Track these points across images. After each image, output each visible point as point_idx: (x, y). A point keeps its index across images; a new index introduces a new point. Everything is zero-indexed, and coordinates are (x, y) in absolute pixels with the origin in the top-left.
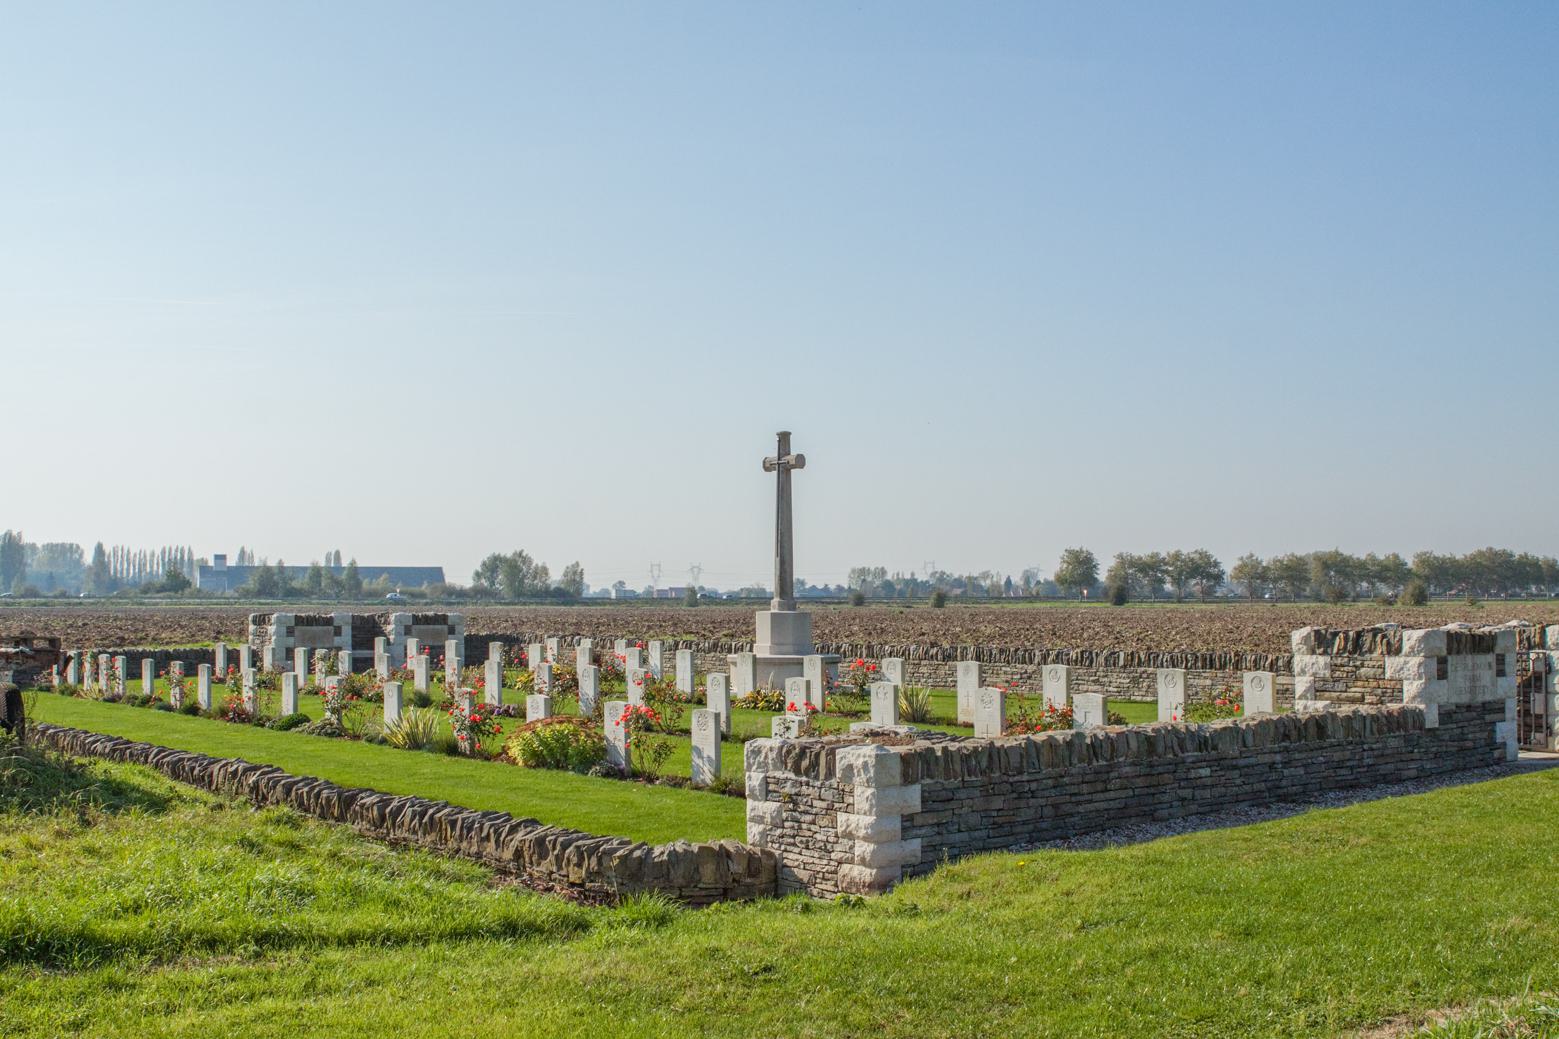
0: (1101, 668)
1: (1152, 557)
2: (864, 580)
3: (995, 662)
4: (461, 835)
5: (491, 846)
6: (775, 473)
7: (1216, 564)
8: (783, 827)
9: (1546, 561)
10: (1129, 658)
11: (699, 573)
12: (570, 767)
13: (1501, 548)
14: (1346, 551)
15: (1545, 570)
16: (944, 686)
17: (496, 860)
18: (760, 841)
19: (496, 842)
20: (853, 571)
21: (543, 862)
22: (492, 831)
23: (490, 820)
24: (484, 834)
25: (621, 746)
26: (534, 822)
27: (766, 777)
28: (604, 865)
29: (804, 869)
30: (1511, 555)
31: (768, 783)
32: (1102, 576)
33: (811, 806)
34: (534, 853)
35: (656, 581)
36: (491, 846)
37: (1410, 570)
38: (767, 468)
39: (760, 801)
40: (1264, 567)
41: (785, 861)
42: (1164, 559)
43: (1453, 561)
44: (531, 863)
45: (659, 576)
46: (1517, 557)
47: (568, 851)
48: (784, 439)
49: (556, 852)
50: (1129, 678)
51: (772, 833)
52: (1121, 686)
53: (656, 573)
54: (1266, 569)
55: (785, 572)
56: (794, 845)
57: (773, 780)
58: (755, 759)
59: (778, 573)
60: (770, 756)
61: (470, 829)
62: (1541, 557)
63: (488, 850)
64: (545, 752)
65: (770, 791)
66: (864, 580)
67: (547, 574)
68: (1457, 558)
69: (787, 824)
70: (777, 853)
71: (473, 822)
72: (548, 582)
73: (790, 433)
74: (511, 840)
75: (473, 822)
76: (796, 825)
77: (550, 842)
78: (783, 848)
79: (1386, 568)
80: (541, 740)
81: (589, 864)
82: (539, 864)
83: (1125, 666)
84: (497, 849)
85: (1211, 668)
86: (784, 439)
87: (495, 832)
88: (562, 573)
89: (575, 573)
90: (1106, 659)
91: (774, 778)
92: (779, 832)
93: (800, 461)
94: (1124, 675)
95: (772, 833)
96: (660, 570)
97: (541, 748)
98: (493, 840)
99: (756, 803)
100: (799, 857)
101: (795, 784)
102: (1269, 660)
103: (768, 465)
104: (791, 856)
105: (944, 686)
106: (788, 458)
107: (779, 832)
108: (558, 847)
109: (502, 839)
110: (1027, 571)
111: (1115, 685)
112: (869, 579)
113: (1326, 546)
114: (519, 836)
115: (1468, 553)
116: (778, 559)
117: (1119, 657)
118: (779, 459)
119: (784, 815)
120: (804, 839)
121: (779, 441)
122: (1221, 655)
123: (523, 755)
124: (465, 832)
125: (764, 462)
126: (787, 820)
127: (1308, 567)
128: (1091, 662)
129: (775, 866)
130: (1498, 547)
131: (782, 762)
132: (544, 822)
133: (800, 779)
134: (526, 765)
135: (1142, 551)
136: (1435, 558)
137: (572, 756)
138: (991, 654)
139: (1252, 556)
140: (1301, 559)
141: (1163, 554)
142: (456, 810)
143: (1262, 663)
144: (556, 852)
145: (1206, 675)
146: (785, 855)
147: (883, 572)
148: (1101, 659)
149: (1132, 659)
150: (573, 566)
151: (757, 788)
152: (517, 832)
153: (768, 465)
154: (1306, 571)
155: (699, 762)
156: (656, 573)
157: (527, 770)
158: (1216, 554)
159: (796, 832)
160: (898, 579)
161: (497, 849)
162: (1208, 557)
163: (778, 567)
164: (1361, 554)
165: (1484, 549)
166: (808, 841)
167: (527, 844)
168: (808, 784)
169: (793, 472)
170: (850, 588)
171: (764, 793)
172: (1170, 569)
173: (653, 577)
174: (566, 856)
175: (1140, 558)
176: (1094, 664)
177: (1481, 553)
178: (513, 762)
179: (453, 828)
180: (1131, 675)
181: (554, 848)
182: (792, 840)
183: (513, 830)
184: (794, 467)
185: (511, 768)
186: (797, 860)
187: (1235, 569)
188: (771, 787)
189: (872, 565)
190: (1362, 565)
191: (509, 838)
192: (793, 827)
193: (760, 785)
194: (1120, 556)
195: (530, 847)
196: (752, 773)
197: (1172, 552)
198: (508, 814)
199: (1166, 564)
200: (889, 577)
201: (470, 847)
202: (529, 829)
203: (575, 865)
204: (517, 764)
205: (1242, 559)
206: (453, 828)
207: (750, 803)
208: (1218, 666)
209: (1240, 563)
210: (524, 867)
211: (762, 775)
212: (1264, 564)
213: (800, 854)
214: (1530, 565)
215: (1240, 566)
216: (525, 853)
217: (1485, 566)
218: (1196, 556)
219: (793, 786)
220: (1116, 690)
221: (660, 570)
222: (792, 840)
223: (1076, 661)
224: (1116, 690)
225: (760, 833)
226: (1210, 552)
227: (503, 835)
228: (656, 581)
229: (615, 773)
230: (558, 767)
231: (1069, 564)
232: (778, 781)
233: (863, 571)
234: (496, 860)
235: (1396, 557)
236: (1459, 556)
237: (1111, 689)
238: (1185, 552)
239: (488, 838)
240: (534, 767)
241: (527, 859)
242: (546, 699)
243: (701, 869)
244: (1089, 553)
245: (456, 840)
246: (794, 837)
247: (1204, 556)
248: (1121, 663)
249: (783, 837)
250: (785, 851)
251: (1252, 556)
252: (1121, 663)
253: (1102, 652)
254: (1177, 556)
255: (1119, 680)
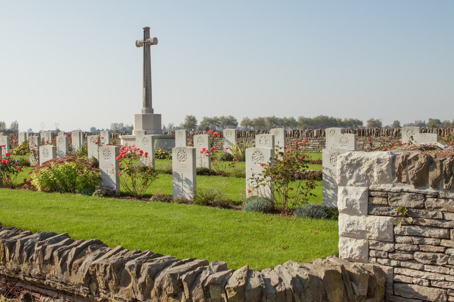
0: (304, 138)
1: (215, 118)
2: (116, 127)
3: (248, 137)
4: (21, 257)
5: (56, 268)
6: (142, 48)
7: (236, 120)
8: (395, 242)
9: (338, 120)
10: (319, 132)
11: (58, 125)
12: (77, 191)
13: (325, 115)
14: (277, 116)
15: (338, 122)
16: (220, 149)
17: (62, 283)
18: (360, 256)
19: (62, 265)
20: (112, 124)
21: (122, 289)
22: (56, 253)
23: (51, 242)
24: (47, 257)
25: (113, 178)
26: (97, 244)
27: (369, 191)
28: (213, 297)
29: (430, 286)
30: (328, 118)
31: (370, 196)
32: (198, 124)
33: (443, 219)
34: (110, 278)
35: (43, 128)
36: (56, 268)
37: (297, 122)
38: (138, 46)
39: (360, 215)
40: (251, 121)
41: (397, 277)
42: (219, 119)
43: (310, 119)
44: (107, 289)
45: (44, 127)
46: (330, 118)
47: (158, 279)
48: (147, 31)
49: (141, 280)
50: (319, 142)
51: (378, 248)
52: (315, 146)
53: (43, 126)
54: (252, 122)
55: (148, 95)
56: (413, 260)
57: (380, 193)
58: (353, 173)
59: (145, 95)
60: (376, 169)
61: (30, 251)
62: (337, 118)
63: (52, 272)
64: (58, 181)
65: (375, 205)
66: (116, 127)
67: (5, 125)
68: (311, 118)
69: (399, 239)
70: (386, 269)
71: (33, 244)
72: (6, 128)
73: (150, 28)
74: (80, 264)
75: (33, 244)
76: (416, 240)
77: (131, 267)
78: (394, 263)
79: (289, 122)
80: (55, 173)
81: (191, 296)
82: (117, 291)
83: (317, 137)
84: (63, 273)
85: (363, 136)
86: (147, 31)
87: (60, 255)
88: (11, 124)
89: (15, 125)
90: (307, 134)
91: (382, 190)
92: (388, 247)
93: (155, 41)
94: (316, 141)
95: (378, 248)
96: (44, 125)
97: (55, 179)
98: (58, 263)
99: (354, 218)
100: (422, 273)
101: (413, 196)
102: (395, 131)
103: (138, 44)
104: (407, 272)
105: (220, 149)
106: (149, 39)
107: (388, 247)
108: (144, 274)
109: (68, 262)
110: (170, 124)
111: (312, 145)
112: (118, 127)
113: (271, 116)
114: (89, 259)
115: (315, 117)
116: (144, 89)
117: (313, 132)
118: (144, 40)
119: (398, 229)
120: (429, 255)
121: (144, 32)
122: (368, 130)
123: (41, 184)
124: (25, 254)
125: (136, 42)
126: (401, 234)
127: (265, 121)
128: (299, 135)
129: (386, 283)
130: (324, 115)
131: (393, 174)
132: (164, 254)
133: (423, 191)
134: (43, 190)
135: (211, 116)
136: (305, 118)
137: (79, 183)
138: (245, 133)
139: (247, 118)
140: (263, 118)
141: (218, 117)
142: (12, 232)
143: (391, 133)
144: (141, 280)
145: (361, 139)
146: (399, 270)
147: (122, 124)
148: (304, 134)
149: (321, 133)
150: (15, 122)
151: (358, 203)
152: (84, 255)
153: (138, 44)
154: (264, 122)
155: (180, 184)
156: (43, 126)
157: (45, 194)
158: (236, 117)
159: (415, 247)
160: (127, 126)
161: (63, 273)
162: (233, 118)
163: (145, 92)
164: (281, 117)
165: (320, 115)
166: (435, 257)
167: (101, 270)
168: (436, 196)
169: (152, 47)
170: (111, 130)
171: (366, 207)
172: (221, 122)
173: (42, 127)
174: (156, 284)
175: (211, 118)
176: (300, 136)
177: (319, 117)
178: (34, 189)
179: (12, 250)
180: (320, 141)
181: (138, 275)
182: (409, 256)
183: (80, 253)
184: (152, 44)
185: (33, 193)
186: (418, 277)
187: (242, 122)
188: (376, 201)
189: (119, 122)
190: (282, 121)
191: (77, 261)
192: (411, 243)
193: (361, 199)
194: (204, 118)
195: (105, 272)
196: (347, 187)
197: (221, 116)
198: (66, 236)
199: (219, 120)
200: (124, 126)
201: (32, 268)
202: (98, 252)
203: (169, 296)
204: (37, 190)
205: (244, 118)
206: (12, 250)
207: (343, 220)
208: (367, 135)
209: (243, 120)
210: (97, 292)
211: (363, 189)
212: (251, 120)
213: (422, 270)
214: (333, 121)
215: (243, 121)
216: (99, 279)
217: (320, 121)
218: (229, 118)
219: (412, 198)
220: (312, 148)
221: (44, 125)
222: (409, 256)
223: (291, 135)
224: (312, 148)
225: (359, 248)
226: (234, 116)
227: (70, 259)
228: (43, 128)
229: (110, 193)
230: (67, 191)
231: (188, 120)
232: (386, 195)
233: (115, 124)
234: (62, 283)
235: (293, 118)
236: (312, 118)
237: (309, 147)
238: (225, 116)
239: (51, 260)
240: (49, 192)
241: (101, 285)
242: (53, 147)
243: (329, 296)
244: (194, 117)
245: (16, 261)
246: (412, 252)
247: (232, 118)
248: (315, 135)
249: (394, 252)
250: (399, 266)
251: (247, 118)
252: (315, 135)
253: (304, 130)
254: (223, 118)
255: (313, 143)
